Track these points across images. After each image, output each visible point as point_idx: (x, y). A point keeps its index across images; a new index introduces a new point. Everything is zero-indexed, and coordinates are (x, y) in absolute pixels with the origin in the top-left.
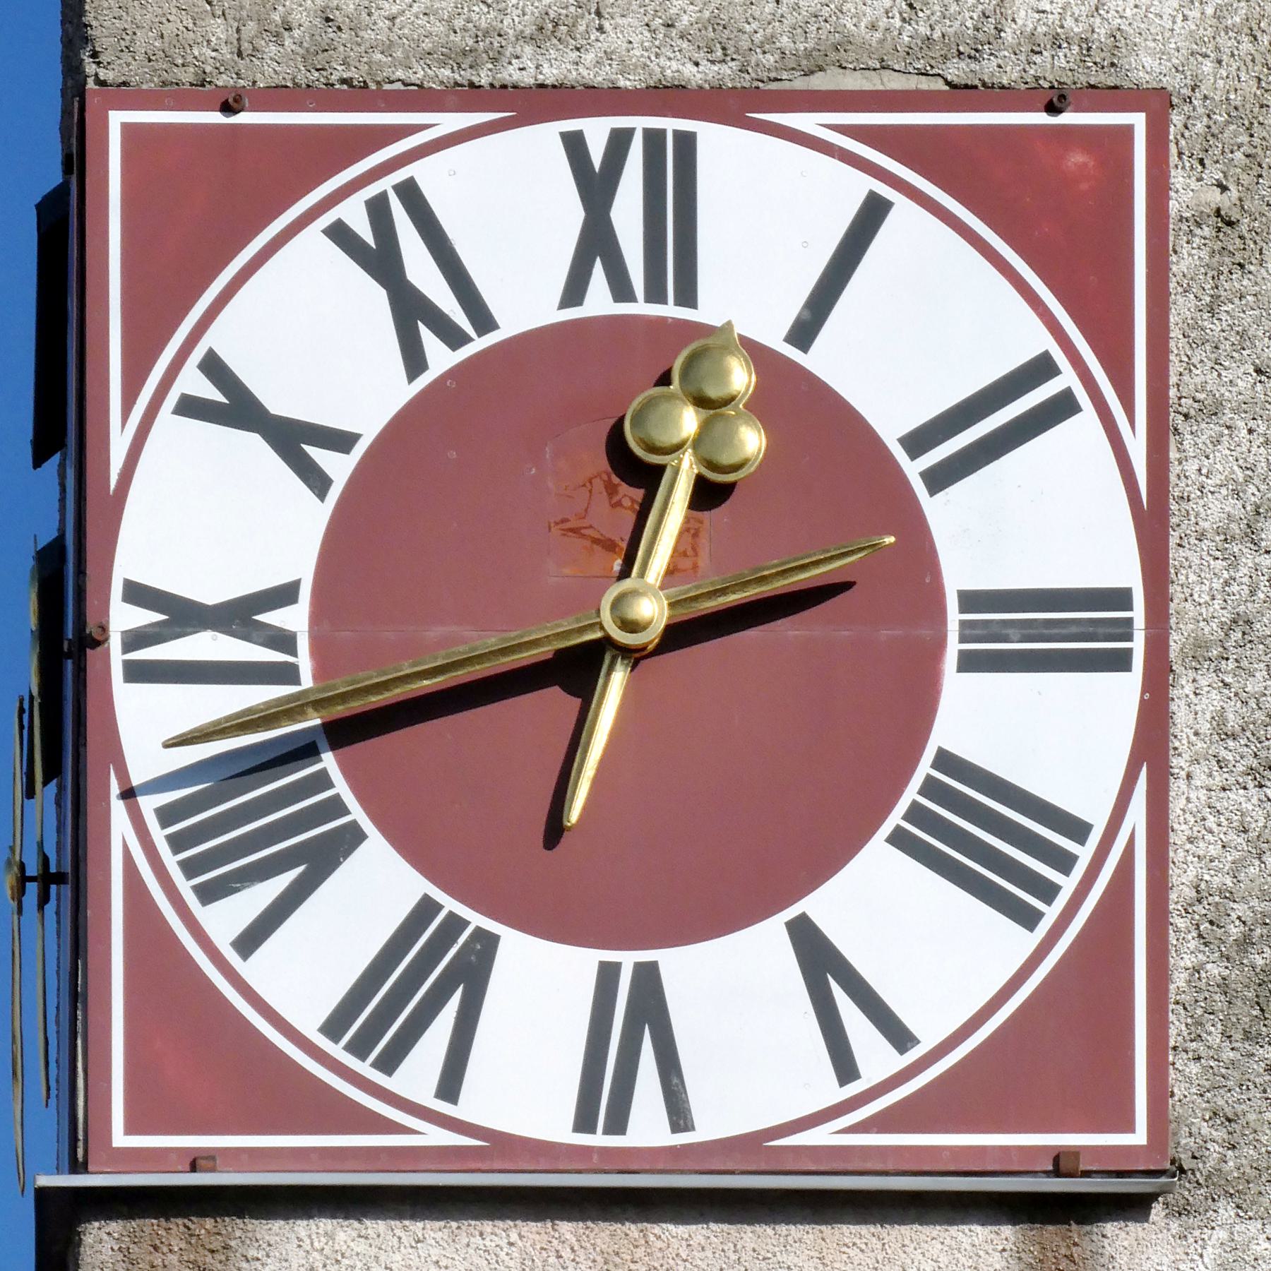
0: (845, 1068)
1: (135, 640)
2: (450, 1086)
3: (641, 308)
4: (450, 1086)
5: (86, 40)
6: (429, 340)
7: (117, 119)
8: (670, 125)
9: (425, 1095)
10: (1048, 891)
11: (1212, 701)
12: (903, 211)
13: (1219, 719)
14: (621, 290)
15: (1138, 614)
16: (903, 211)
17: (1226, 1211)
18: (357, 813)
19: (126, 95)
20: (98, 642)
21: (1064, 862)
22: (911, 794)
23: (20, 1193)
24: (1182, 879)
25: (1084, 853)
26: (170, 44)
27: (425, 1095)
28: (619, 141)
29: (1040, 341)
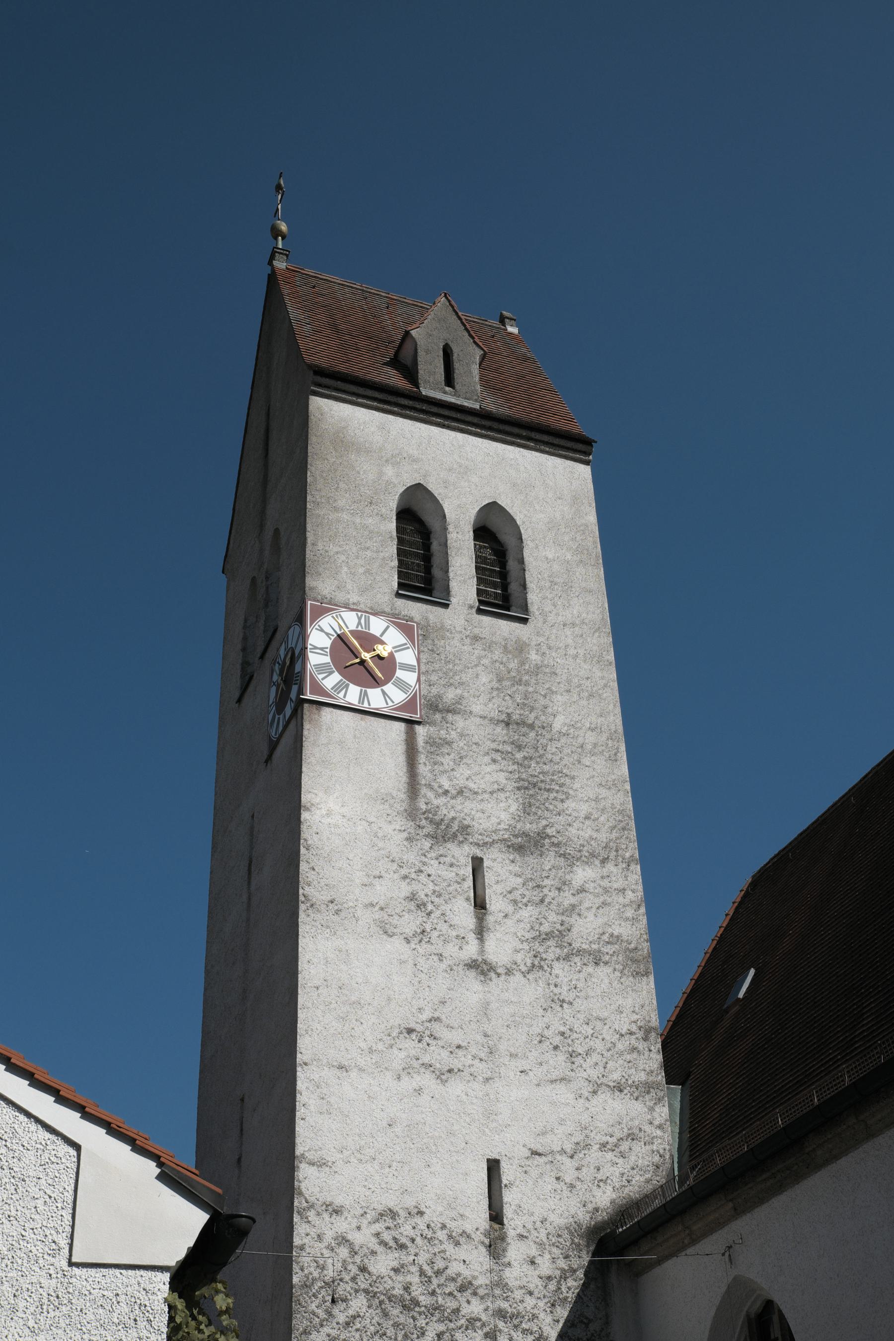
0: (387, 704)
1: (310, 649)
2: (345, 696)
3: (364, 630)
4: (345, 696)
5: (271, 760)
6: (360, 626)
7: (309, 602)
8: (367, 615)
9: (342, 697)
10: (408, 691)
11: (424, 678)
12: (391, 627)
13: (425, 680)
14: (362, 628)
15: (417, 668)
16: (391, 627)
17: (428, 725)
18: (334, 669)
19: (310, 600)
20: (307, 648)
21: (410, 689)
22: (393, 679)
23: (274, 215)
24: (422, 693)
25: (412, 689)
26: (26, 1276)
27: (342, 697)
28: (362, 615)
29: (406, 642)
